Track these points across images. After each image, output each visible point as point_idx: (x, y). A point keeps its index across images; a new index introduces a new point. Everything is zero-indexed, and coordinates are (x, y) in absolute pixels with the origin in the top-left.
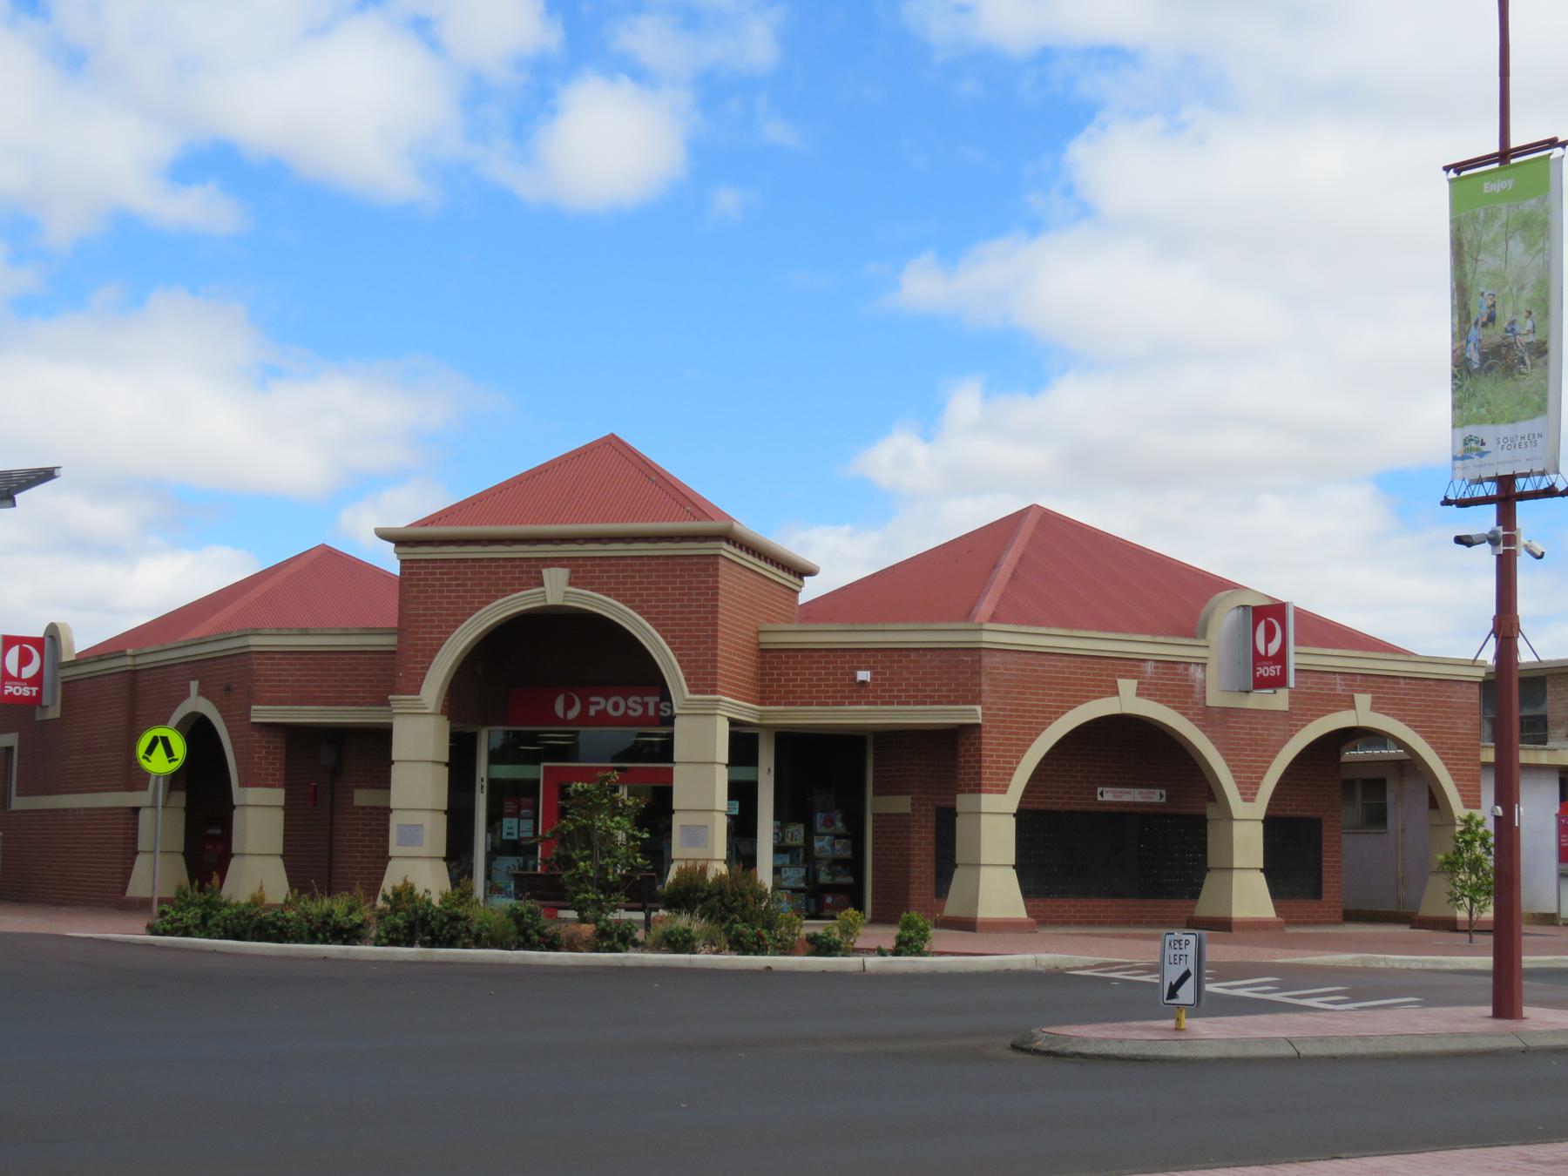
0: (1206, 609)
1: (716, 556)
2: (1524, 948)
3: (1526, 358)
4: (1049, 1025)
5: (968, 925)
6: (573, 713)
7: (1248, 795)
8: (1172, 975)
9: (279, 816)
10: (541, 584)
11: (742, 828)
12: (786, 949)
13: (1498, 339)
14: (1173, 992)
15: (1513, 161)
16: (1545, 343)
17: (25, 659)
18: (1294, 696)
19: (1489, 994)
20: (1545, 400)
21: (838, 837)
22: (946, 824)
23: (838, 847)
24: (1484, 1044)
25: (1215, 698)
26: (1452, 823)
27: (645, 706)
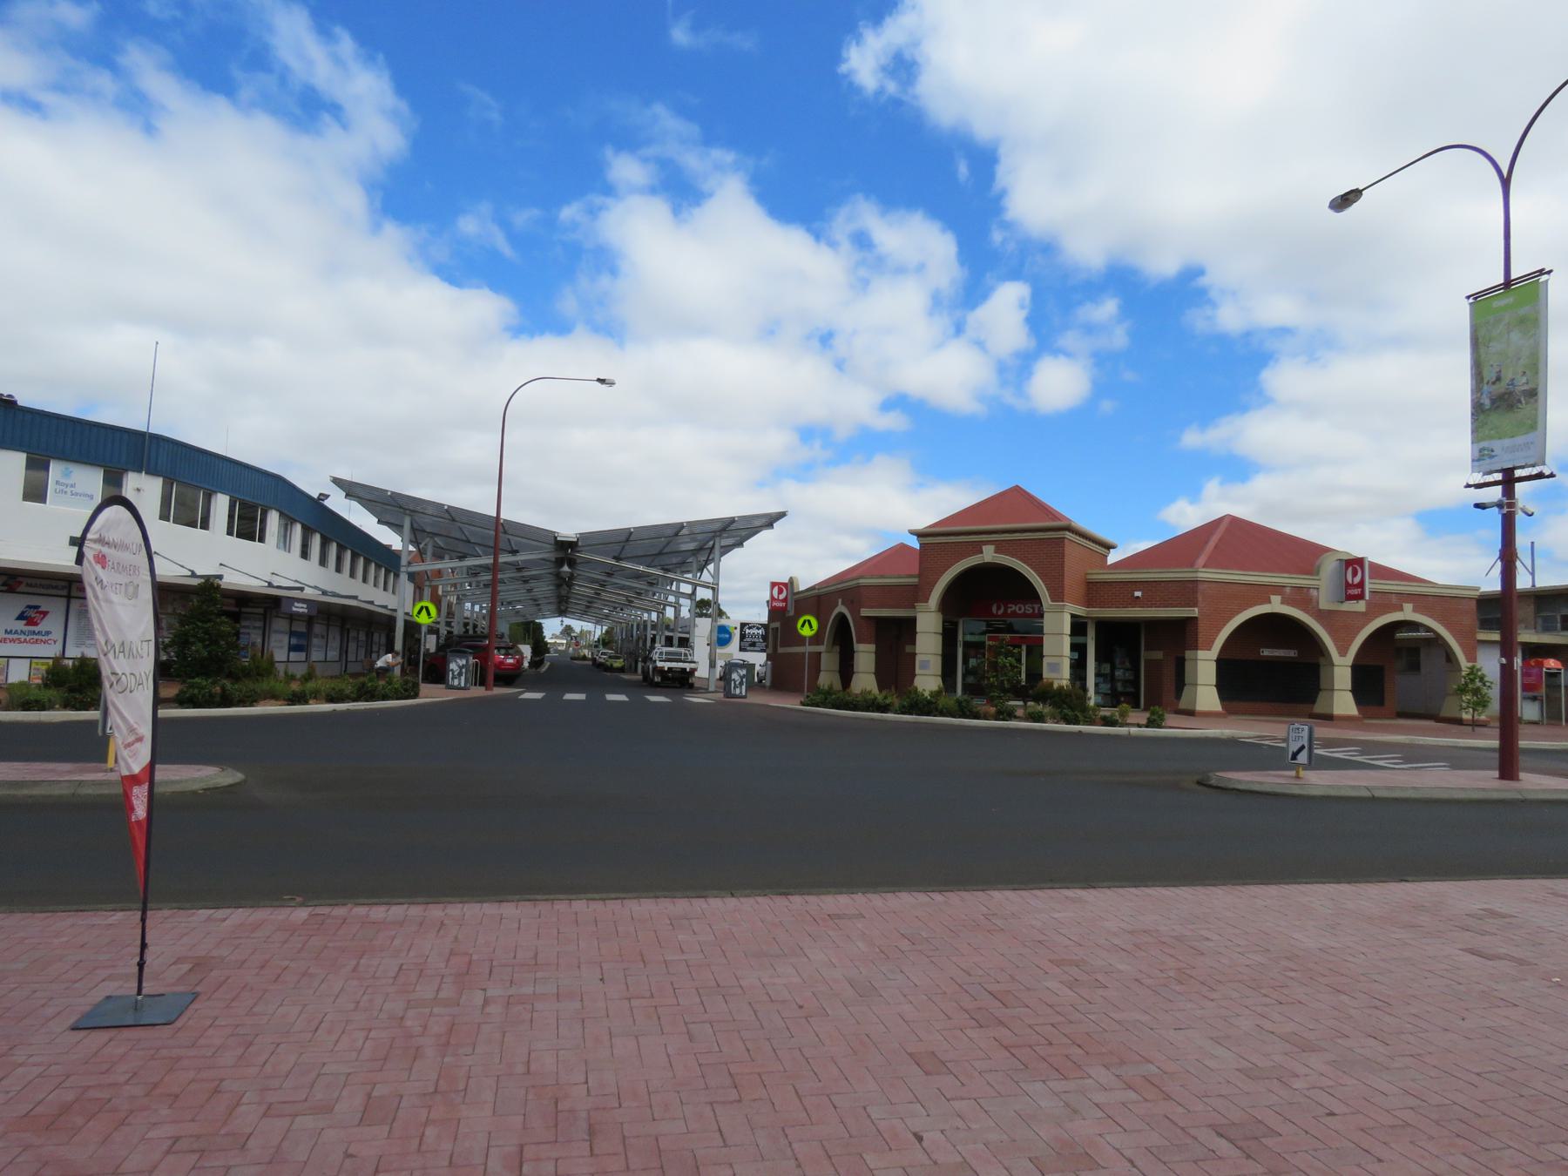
0: (1321, 558)
1: (1064, 538)
2: (1520, 737)
3: (1522, 399)
4: (1218, 771)
5: (1191, 713)
6: (1001, 612)
7: (1343, 652)
8: (1294, 747)
9: (873, 656)
10: (982, 553)
11: (1078, 666)
12: (1092, 723)
13: (1503, 390)
14: (1294, 756)
15: (1513, 287)
16: (1536, 389)
17: (780, 591)
18: (1369, 604)
19: (1496, 763)
20: (1536, 423)
21: (1127, 670)
22: (1180, 665)
23: (1127, 675)
24: (1495, 796)
25: (1324, 605)
26: (1460, 670)
27: (1033, 608)
